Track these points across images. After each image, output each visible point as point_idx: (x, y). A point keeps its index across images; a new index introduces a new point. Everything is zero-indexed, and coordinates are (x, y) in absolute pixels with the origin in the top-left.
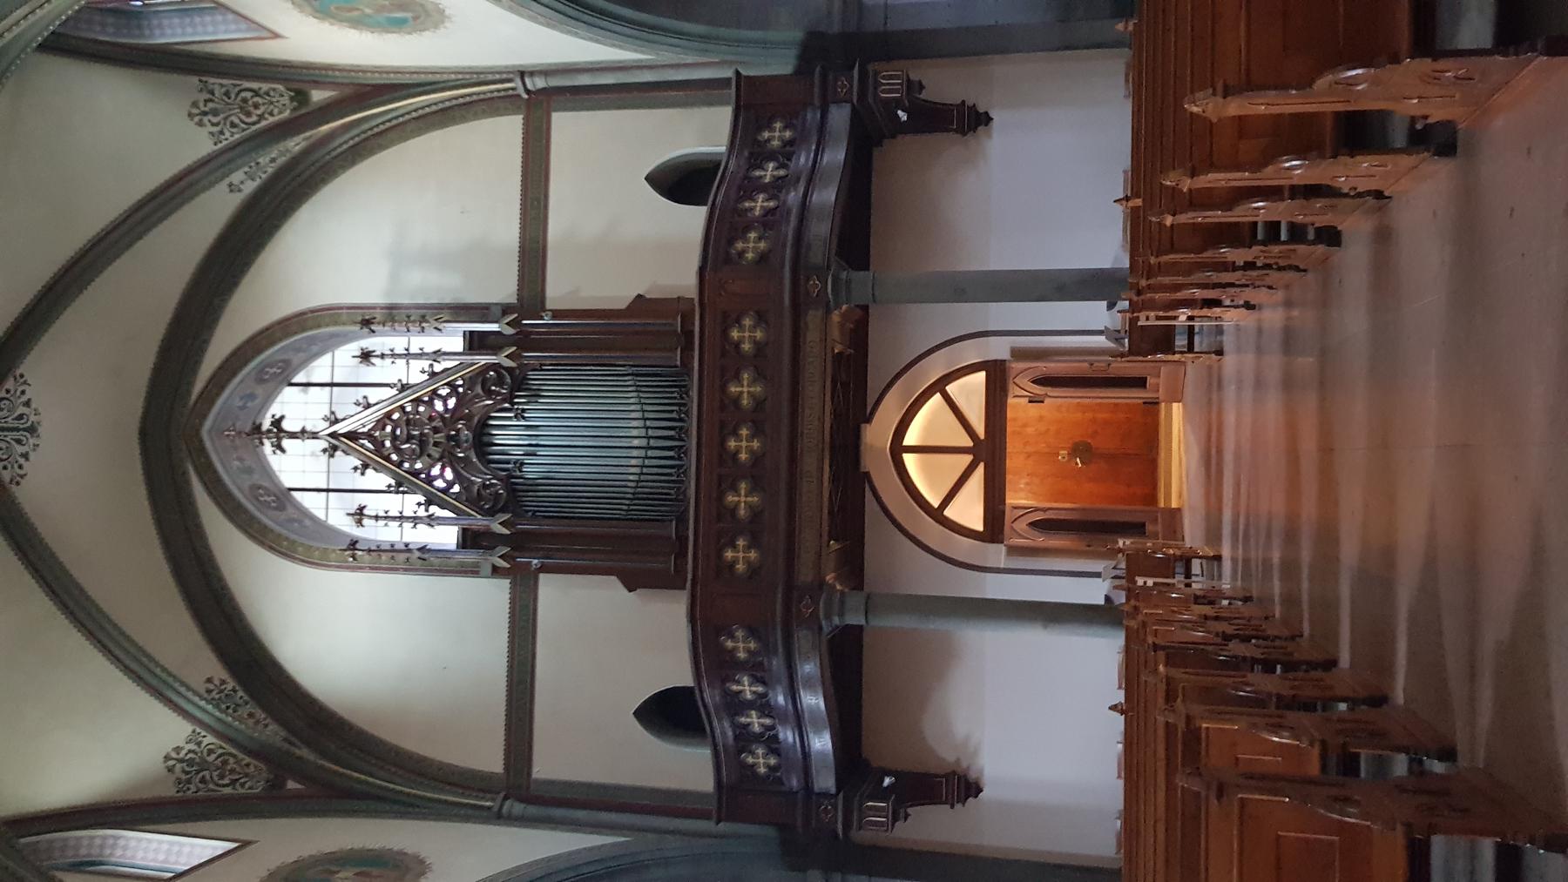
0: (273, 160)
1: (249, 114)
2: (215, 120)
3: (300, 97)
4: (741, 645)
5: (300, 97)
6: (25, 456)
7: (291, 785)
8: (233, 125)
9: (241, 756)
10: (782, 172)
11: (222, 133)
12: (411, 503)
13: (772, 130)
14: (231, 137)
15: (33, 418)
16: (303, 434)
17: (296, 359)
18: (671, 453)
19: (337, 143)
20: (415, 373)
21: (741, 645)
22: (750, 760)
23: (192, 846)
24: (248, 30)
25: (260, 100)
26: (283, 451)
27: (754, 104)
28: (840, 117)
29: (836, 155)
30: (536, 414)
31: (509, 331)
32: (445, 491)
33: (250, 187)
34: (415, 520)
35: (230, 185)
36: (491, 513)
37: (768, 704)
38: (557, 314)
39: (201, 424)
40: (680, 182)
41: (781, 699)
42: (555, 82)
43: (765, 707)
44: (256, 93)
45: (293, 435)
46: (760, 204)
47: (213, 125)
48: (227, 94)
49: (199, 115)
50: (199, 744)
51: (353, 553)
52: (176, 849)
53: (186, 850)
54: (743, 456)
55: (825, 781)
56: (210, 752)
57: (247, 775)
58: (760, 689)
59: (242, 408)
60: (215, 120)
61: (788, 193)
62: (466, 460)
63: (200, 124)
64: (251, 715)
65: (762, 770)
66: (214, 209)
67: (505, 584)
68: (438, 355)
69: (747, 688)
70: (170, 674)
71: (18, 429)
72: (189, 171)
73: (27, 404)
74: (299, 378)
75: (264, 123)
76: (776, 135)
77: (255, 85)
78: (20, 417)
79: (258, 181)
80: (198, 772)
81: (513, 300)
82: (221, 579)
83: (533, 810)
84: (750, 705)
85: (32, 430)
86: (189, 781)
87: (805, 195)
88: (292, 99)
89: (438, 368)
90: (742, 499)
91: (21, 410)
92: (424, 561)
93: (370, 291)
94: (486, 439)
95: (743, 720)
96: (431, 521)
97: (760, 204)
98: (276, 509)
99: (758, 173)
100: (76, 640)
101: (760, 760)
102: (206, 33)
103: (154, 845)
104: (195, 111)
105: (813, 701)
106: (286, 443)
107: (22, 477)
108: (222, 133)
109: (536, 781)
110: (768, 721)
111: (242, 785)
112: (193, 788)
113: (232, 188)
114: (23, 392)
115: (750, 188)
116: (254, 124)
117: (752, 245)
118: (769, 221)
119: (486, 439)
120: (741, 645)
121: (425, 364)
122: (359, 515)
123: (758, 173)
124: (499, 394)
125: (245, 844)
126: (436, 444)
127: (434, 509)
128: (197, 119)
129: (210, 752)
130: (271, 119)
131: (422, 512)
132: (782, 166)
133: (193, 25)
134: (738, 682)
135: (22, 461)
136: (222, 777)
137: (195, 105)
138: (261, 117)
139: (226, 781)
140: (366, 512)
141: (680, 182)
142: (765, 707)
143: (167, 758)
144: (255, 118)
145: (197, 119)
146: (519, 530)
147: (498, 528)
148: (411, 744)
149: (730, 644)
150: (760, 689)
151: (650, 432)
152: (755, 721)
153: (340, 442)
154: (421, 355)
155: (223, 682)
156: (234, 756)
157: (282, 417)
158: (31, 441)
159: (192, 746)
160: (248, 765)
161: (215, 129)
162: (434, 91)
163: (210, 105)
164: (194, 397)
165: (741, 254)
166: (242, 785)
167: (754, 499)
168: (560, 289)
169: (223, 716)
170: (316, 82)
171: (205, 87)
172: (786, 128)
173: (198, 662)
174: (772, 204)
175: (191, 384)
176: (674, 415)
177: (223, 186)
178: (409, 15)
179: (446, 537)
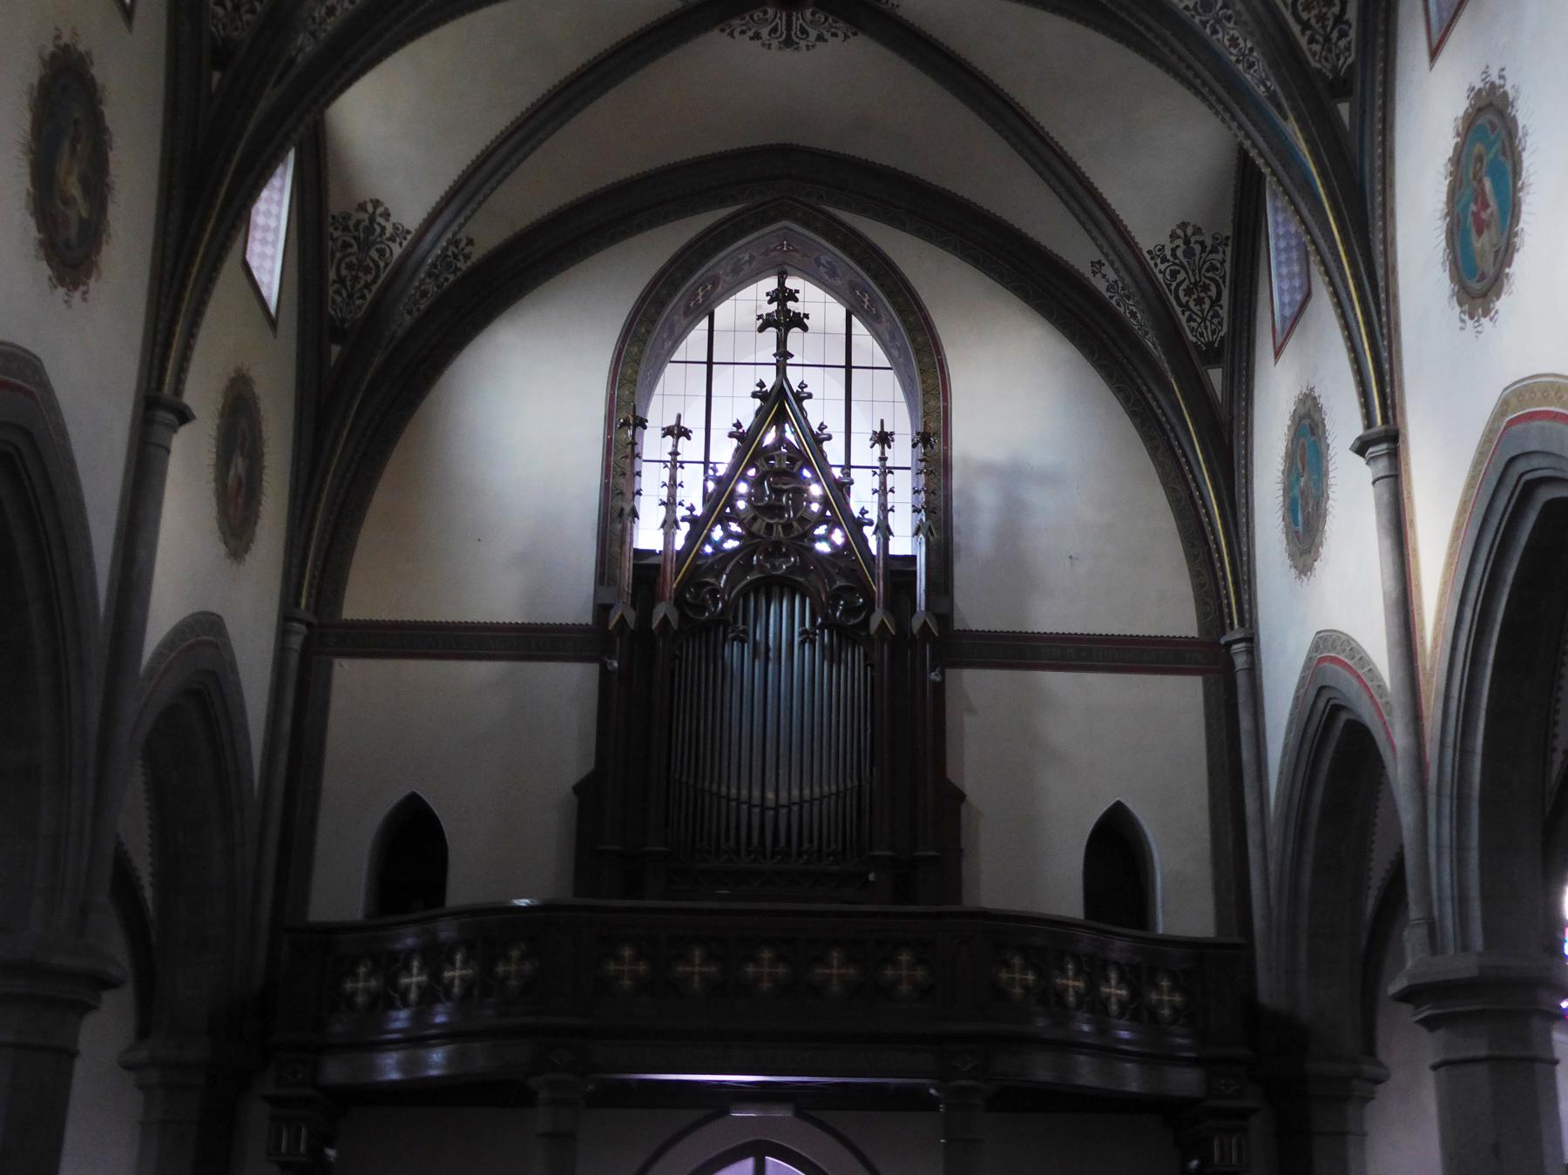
0: (1133, 315)
1: (1188, 292)
2: (1179, 253)
3: (1213, 355)
4: (513, 968)
5: (1213, 355)
6: (757, 36)
7: (336, 350)
8: (1174, 274)
9: (374, 288)
10: (1114, 1008)
11: (1164, 260)
12: (692, 495)
13: (1172, 990)
14: (1160, 270)
15: (803, 43)
16: (783, 355)
17: (881, 328)
18: (755, 840)
19: (1160, 396)
20: (862, 498)
21: (513, 967)
22: (362, 970)
23: (273, 258)
24: (1284, 318)
25: (1206, 306)
26: (761, 329)
27: (1215, 965)
28: (1185, 1082)
29: (1132, 1079)
30: (805, 659)
31: (916, 624)
32: (708, 539)
33: (1101, 285)
34: (670, 504)
35: (1099, 262)
36: (679, 601)
37: (436, 1000)
38: (939, 689)
39: (796, 220)
40: (1116, 845)
41: (440, 1019)
42: (1242, 680)
43: (432, 994)
44: (1216, 302)
45: (782, 342)
46: (1072, 983)
47: (1174, 250)
48: (1213, 268)
49: (1185, 234)
50: (392, 239)
51: (624, 419)
52: (270, 237)
53: (269, 251)
54: (750, 969)
55: (335, 1071)
56: (381, 252)
57: (350, 296)
58: (456, 990)
59: (819, 263)
60: (1179, 253)
61: (1089, 1022)
62: (749, 568)
63: (1173, 236)
64: (424, 294)
65: (349, 986)
66: (1075, 248)
67: (587, 618)
68: (884, 531)
69: (456, 973)
70: (480, 204)
71: (789, 28)
72: (1115, 221)
73: (820, 38)
74: (858, 326)
75: (1178, 310)
76: (1165, 997)
77: (1225, 301)
78: (803, 31)
79: (1107, 295)
80: (355, 238)
81: (958, 625)
82: (598, 248)
83: (294, 660)
84: (435, 976)
85: (788, 42)
86: (346, 229)
87: (1086, 1046)
88: (1210, 344)
89: (868, 531)
90: (696, 968)
91: (813, 34)
92: (616, 510)
93: (971, 438)
94: (776, 590)
95: (416, 964)
96: (669, 525)
97: (1072, 983)
98: (688, 307)
99: (1113, 976)
100: (526, 97)
101: (362, 984)
102: (1279, 264)
103: (274, 209)
104: (1190, 231)
105: (437, 1060)
106: (771, 333)
107: (731, 34)
108: (1164, 260)
109: (330, 666)
110: (413, 996)
111: (338, 292)
112: (336, 234)
113: (1097, 266)
114: (835, 35)
115: (1094, 969)
116: (1177, 298)
117: (1019, 977)
118: (1051, 999)
119: (776, 590)
120: (513, 968)
121: (873, 515)
122: (678, 431)
123: (1113, 976)
124: (835, 609)
125: (273, 323)
126: (769, 527)
127: (685, 527)
128: (1180, 232)
129: (381, 252)
130: (1183, 319)
131: (681, 512)
132: (1123, 1005)
133: (1289, 261)
134: (465, 963)
135: (750, 33)
136: (350, 267)
137: (1198, 231)
138: (1185, 307)
139: (344, 272)
140: (683, 439)
141: (1116, 845)
142: (432, 994)
143: (377, 203)
144: (1184, 300)
145: (1180, 232)
146: (654, 635)
147: (661, 611)
148: (381, 498)
149: (515, 953)
150: (456, 990)
151: (784, 811)
152: (414, 979)
153: (779, 402)
154: (884, 509)
155: (467, 257)
156: (374, 281)
157: (805, 328)
158: (775, 43)
159: (389, 230)
160: (363, 297)
161: (1168, 253)
162: (1225, 525)
163: (1197, 248)
164: (832, 210)
165: (1007, 964)
166: (338, 292)
167: (696, 983)
168: (978, 691)
169: (425, 268)
170: (1232, 373)
171: (1219, 243)
172: (1174, 1008)
173: (488, 231)
174: (1071, 999)
175: (847, 207)
176: (806, 846)
177: (1098, 256)
178: (1300, 528)
179: (648, 535)
